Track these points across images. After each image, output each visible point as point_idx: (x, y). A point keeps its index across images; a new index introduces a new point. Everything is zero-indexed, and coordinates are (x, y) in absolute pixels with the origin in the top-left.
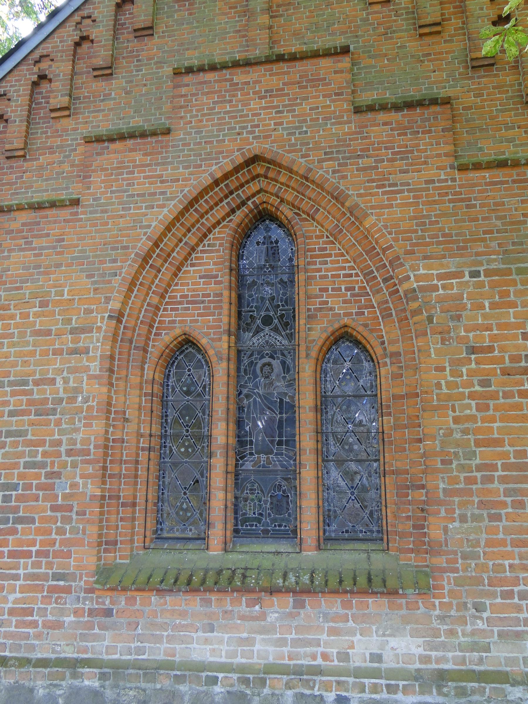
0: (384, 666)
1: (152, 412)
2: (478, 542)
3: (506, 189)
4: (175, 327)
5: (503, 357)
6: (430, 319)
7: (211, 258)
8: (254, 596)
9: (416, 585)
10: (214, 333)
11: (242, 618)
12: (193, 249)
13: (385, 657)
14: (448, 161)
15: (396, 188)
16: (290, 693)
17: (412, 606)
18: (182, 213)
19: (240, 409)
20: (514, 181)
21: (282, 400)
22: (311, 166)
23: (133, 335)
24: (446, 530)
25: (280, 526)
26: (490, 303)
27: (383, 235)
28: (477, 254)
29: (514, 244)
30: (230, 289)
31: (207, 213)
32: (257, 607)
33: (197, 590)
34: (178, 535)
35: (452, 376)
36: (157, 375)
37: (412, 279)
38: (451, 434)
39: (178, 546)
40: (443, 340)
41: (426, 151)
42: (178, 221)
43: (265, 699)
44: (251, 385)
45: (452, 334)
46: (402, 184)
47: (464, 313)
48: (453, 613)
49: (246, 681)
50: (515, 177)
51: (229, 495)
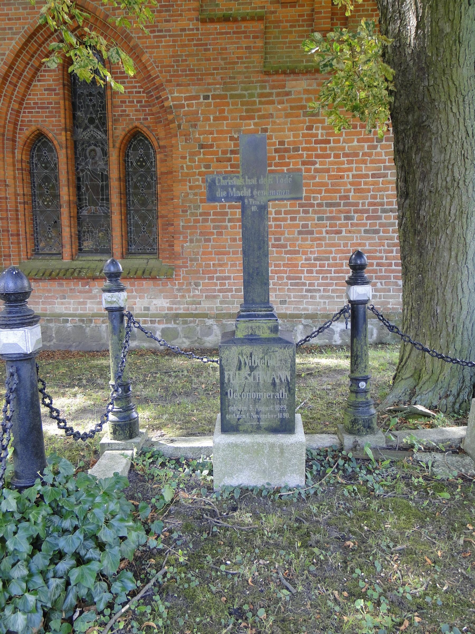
0: (150, 312)
1: (23, 180)
2: (198, 252)
3: (229, 38)
4: (32, 125)
5: (218, 151)
6: (179, 126)
7: (51, 76)
8: (84, 281)
9: (166, 274)
10: (57, 130)
11: (80, 292)
12: (38, 70)
13: (151, 308)
14: (194, 14)
15: (162, 34)
16: (104, 325)
17: (165, 285)
18: (26, 44)
19: (79, 179)
20: (234, 33)
21: (102, 173)
22: (108, 13)
23: (4, 131)
24: (183, 247)
25: (104, 246)
26: (214, 117)
27: (153, 69)
28: (209, 84)
29: (230, 78)
30: (65, 99)
31: (43, 43)
32: (87, 287)
33: (55, 279)
34: (47, 252)
35: (189, 162)
36: (24, 156)
37: (170, 99)
38: (188, 196)
39: (47, 258)
40: (186, 140)
41: (181, 5)
42: (24, 49)
43: (92, 328)
44: (83, 164)
45: (191, 136)
46: (166, 31)
47: (199, 123)
48: (184, 287)
49: (83, 321)
50: (235, 30)
51: (73, 230)
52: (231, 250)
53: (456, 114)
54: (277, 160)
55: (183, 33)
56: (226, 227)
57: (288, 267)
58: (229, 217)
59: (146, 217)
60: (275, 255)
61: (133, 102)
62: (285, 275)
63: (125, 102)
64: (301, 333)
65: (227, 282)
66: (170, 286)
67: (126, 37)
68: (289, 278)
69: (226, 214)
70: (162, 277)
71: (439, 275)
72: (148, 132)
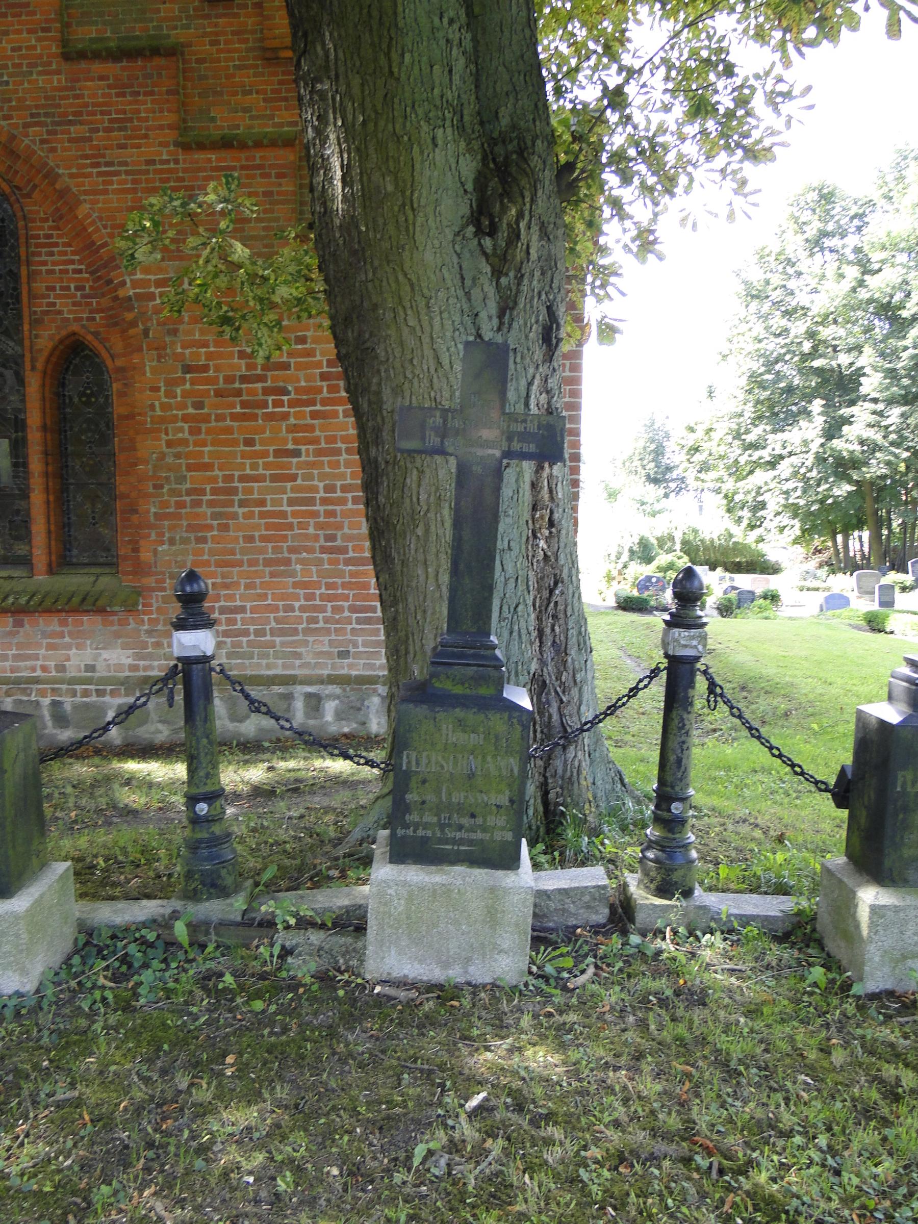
0: (97, 675)
5: (217, 377)
6: (146, 332)
13: (98, 668)
17: (123, 623)
21: (16, 417)
22: (15, 132)
24: (155, 552)
35: (166, 397)
37: (129, 284)
40: (159, 357)
41: (146, 119)
45: (168, 351)
46: (121, 164)
47: (181, 327)
48: (159, 627)
50: (244, 163)
52: (245, 558)
53: (414, 329)
54: (325, 394)
55: (151, 168)
56: (234, 516)
57: (351, 589)
58: (241, 496)
59: (98, 497)
60: (326, 566)
61: (68, 288)
62: (346, 604)
63: (53, 289)
64: (377, 711)
65: (239, 616)
66: (133, 625)
67: (46, 176)
68: (353, 609)
69: (234, 491)
70: (117, 608)
71: (413, 608)
72: (96, 343)
